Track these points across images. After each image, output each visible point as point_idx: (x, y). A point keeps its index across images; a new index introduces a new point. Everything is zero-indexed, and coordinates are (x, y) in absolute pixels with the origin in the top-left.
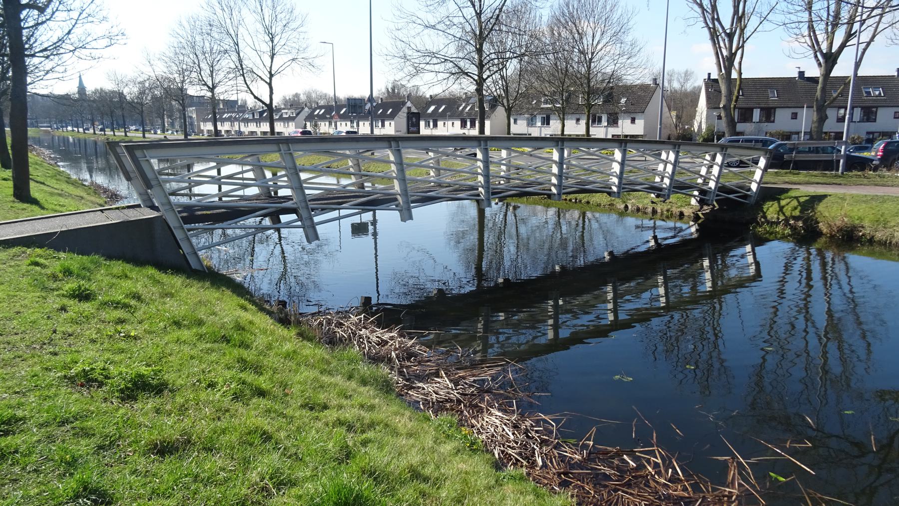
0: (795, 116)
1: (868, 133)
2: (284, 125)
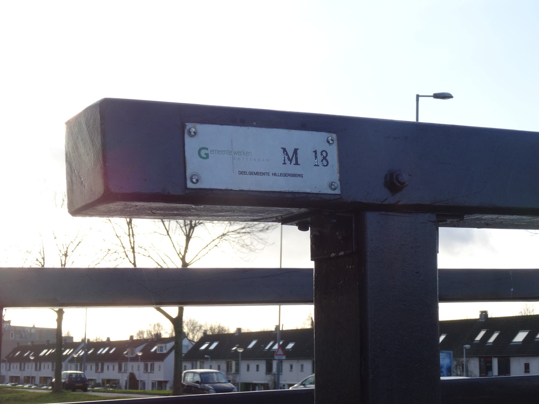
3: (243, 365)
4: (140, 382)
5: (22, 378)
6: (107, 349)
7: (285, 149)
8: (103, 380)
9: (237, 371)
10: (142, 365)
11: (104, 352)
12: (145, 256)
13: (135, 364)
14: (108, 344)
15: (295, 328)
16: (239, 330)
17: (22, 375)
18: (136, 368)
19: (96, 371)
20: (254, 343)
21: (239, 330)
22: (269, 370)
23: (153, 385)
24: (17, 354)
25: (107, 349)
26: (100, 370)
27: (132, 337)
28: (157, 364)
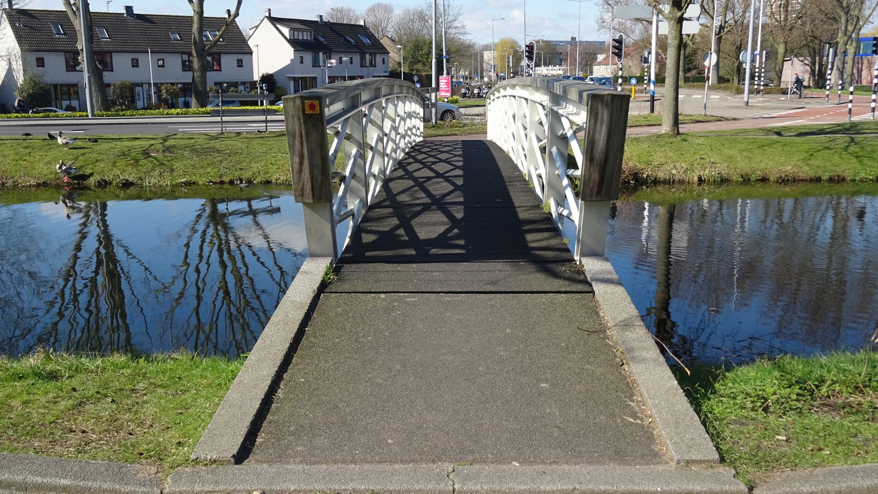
0: (135, 64)
1: (216, 84)
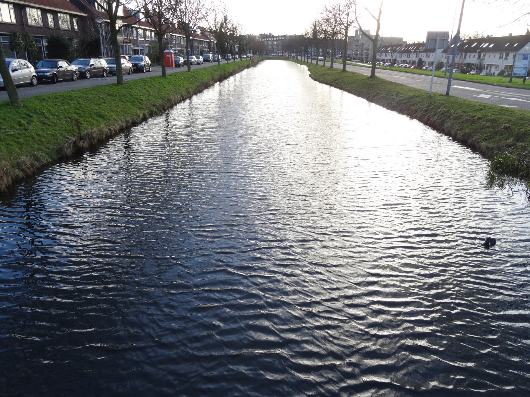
2: (501, 57)
3: (468, 55)
4: (121, 47)
5: (408, 61)
6: (487, 44)
7: (202, 92)
8: (410, 61)
9: (465, 57)
10: (425, 54)
11: (485, 46)
12: (382, 4)
13: (423, 54)
14: (489, 40)
15: (501, 36)
16: (511, 34)
17: (408, 60)
18: (423, 56)
19: (427, 57)
20: (475, 44)
21: (511, 34)
22: (479, 57)
23: (429, 63)
24: (515, 45)
25: (487, 44)
26: (504, 58)
27: (424, 42)
28: (431, 54)
